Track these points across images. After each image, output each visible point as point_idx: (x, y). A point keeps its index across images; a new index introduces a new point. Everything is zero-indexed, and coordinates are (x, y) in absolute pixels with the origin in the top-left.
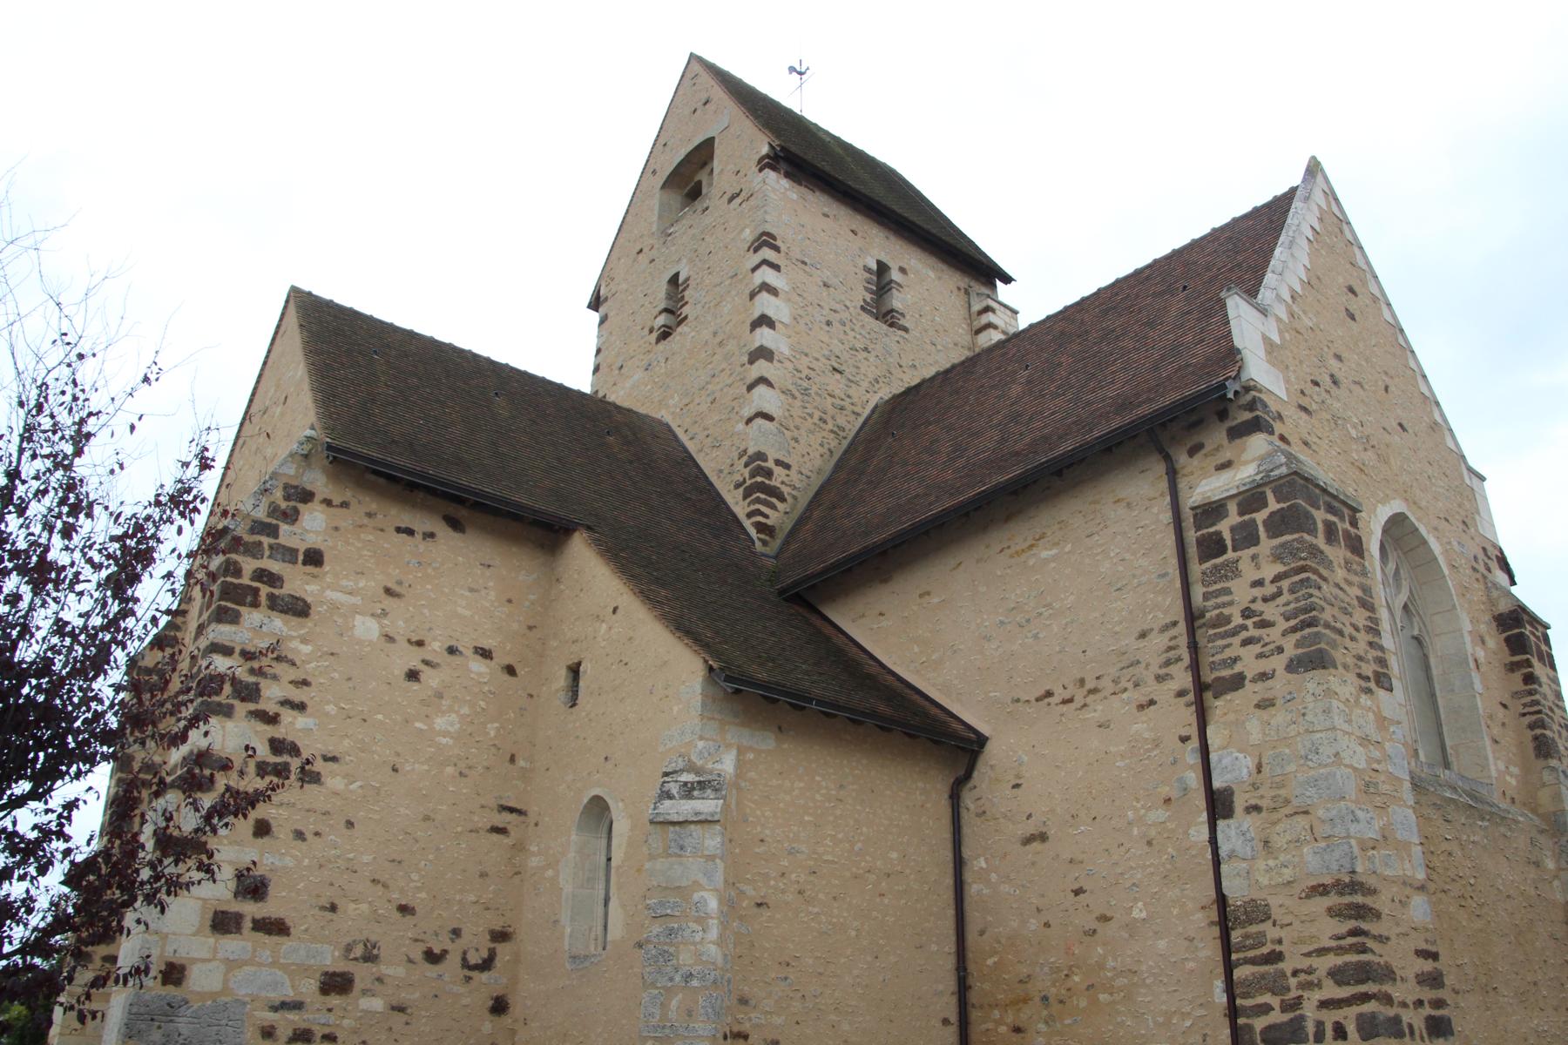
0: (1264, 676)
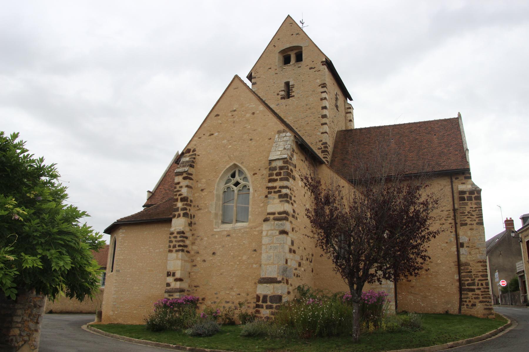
0: (471, 224)
